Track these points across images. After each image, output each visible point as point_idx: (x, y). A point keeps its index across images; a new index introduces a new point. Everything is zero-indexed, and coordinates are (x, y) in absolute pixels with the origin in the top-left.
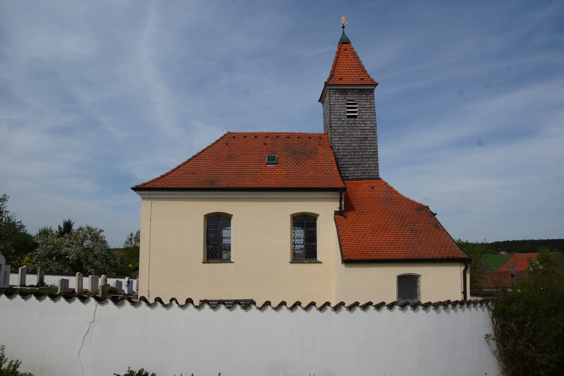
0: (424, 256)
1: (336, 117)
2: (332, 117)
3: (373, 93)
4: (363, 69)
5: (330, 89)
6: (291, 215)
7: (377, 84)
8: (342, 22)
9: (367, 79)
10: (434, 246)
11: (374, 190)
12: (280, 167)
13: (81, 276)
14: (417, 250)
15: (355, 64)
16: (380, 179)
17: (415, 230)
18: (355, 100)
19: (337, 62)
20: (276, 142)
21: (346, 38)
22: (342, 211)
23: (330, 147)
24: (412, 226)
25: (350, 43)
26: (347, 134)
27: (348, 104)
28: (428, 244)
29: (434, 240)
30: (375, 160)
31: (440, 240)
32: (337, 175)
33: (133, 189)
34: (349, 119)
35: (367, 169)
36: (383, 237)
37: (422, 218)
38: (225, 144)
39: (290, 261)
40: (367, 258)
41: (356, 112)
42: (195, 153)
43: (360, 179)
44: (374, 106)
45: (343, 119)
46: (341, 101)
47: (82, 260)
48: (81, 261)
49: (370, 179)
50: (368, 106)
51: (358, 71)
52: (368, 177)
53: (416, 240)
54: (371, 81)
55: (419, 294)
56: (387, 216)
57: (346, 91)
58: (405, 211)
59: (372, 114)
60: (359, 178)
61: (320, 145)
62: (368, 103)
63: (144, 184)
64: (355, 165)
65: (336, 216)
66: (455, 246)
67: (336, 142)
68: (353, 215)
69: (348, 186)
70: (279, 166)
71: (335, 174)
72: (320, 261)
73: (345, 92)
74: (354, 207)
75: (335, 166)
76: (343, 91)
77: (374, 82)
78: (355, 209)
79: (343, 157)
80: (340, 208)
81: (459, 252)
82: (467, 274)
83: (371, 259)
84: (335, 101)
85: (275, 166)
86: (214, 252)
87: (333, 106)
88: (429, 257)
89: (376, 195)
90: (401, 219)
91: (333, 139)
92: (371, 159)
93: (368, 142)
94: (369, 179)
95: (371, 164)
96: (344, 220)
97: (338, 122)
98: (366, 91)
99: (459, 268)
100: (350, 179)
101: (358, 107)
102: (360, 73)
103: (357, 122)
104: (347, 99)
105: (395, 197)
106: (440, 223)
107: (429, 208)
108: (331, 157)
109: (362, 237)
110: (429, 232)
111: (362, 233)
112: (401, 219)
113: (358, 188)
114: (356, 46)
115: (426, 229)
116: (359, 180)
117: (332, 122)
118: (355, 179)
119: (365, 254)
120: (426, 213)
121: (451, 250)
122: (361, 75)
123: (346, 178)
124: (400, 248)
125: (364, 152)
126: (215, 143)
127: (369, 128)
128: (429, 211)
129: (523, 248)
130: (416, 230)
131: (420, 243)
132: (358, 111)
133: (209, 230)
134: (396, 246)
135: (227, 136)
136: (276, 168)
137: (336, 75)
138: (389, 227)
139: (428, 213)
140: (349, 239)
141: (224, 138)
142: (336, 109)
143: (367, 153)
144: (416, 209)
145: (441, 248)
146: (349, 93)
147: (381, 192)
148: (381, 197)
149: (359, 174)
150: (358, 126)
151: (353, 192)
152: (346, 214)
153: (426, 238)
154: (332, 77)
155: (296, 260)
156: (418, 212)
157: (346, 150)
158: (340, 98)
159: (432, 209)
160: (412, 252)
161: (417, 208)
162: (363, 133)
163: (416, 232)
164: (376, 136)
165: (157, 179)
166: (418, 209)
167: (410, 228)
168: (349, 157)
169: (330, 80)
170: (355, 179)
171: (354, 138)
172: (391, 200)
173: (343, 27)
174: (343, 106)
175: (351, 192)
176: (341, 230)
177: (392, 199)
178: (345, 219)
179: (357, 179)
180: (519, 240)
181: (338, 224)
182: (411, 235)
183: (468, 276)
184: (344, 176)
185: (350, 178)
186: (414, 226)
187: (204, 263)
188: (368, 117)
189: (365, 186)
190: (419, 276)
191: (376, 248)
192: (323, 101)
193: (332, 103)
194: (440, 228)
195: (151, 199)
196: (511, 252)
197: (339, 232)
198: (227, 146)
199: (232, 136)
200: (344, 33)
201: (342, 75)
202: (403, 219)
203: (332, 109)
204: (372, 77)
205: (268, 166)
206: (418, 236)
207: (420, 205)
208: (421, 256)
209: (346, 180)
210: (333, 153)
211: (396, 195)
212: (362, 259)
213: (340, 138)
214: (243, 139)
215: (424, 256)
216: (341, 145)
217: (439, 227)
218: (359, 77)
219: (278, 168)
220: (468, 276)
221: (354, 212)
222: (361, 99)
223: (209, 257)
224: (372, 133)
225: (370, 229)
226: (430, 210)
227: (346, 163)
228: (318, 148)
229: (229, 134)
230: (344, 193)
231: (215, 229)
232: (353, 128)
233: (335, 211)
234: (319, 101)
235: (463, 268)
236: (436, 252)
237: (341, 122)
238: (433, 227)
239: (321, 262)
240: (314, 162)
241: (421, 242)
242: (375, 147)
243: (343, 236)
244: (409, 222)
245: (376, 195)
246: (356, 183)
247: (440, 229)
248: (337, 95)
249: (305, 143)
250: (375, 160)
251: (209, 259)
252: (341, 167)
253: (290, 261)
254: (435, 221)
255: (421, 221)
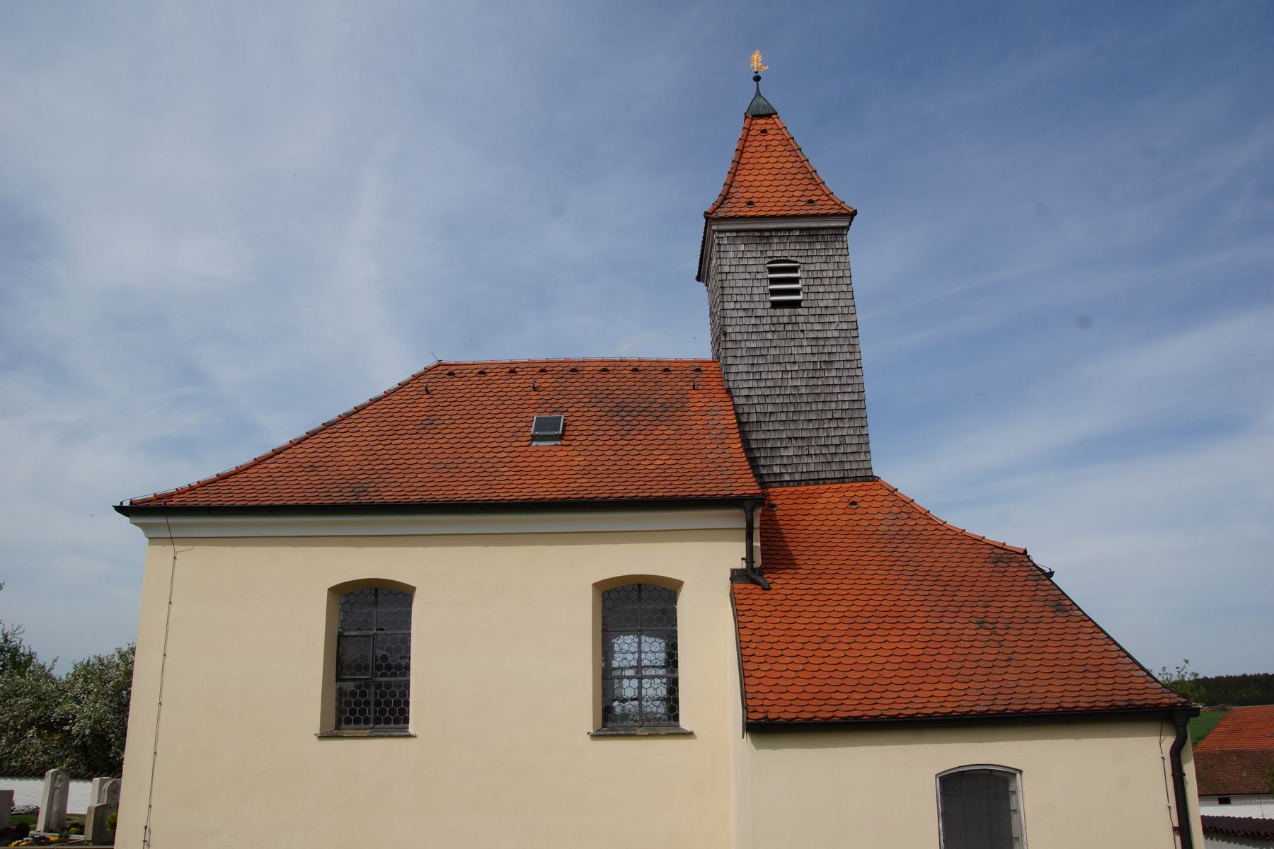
0: (1029, 701)
1: (738, 306)
2: (727, 306)
3: (843, 238)
4: (813, 178)
5: (720, 231)
6: (597, 586)
7: (855, 213)
8: (753, 68)
9: (826, 203)
10: (1057, 669)
11: (857, 511)
12: (570, 445)
13: (60, 780)
14: (1003, 684)
15: (790, 165)
16: (874, 479)
17: (991, 620)
18: (793, 259)
19: (739, 163)
20: (570, 384)
21: (765, 103)
22: (754, 570)
23: (725, 391)
24: (978, 609)
25: (776, 114)
26: (773, 352)
27: (772, 270)
28: (1037, 663)
29: (1057, 650)
30: (858, 423)
31: (1076, 648)
32: (742, 464)
33: (120, 509)
34: (779, 312)
35: (834, 451)
36: (885, 646)
37: (1009, 584)
38: (421, 393)
39: (592, 731)
40: (831, 715)
41: (796, 292)
42: (333, 416)
43: (816, 481)
44: (847, 273)
45: (760, 313)
46: (752, 262)
47: (111, 736)
48: (107, 739)
49: (846, 480)
50: (830, 274)
51: (798, 182)
52: (837, 475)
53: (996, 651)
54: (836, 207)
55: (1017, 839)
56: (898, 582)
57: (767, 234)
58: (955, 565)
59: (843, 295)
60: (812, 478)
61: (694, 389)
62: (831, 266)
63: (158, 498)
64: (799, 440)
65: (737, 586)
66: (1130, 667)
67: (740, 377)
68: (789, 581)
69: (781, 502)
70: (568, 443)
71: (733, 460)
72: (688, 729)
73: (764, 236)
74: (795, 557)
75: (735, 441)
76: (757, 234)
77: (845, 209)
78: (798, 563)
79: (761, 418)
80: (749, 558)
81: (1148, 685)
82: (1187, 763)
83: (842, 718)
84: (735, 262)
85: (556, 445)
86: (358, 703)
87: (730, 277)
88: (1044, 706)
89: (863, 523)
90: (942, 588)
91: (733, 367)
92: (846, 421)
93: (833, 373)
94: (842, 480)
95: (846, 437)
96: (761, 597)
97: (746, 321)
98: (823, 232)
99: (1156, 739)
100: (786, 481)
101: (801, 278)
102: (806, 187)
103: (801, 319)
104: (769, 257)
105: (922, 528)
106: (1068, 598)
107: (1028, 554)
108: (726, 417)
109: (816, 646)
110: (1035, 626)
111: (816, 632)
112: (942, 588)
113: (811, 506)
114: (792, 119)
115: (1026, 615)
116: (812, 482)
117: (728, 321)
118: (799, 482)
119: (823, 702)
120: (1020, 569)
121: (1117, 680)
122: (807, 193)
123: (773, 480)
124: (944, 679)
125: (824, 402)
126: (395, 391)
127: (836, 334)
128: (1030, 564)
129: (1244, 695)
130: (995, 621)
131: (1010, 659)
132: (801, 289)
133: (346, 633)
134: (931, 672)
135: (433, 372)
136: (559, 448)
137: (738, 195)
138: (904, 614)
139: (1028, 569)
140: (772, 652)
141: (423, 377)
142: (740, 283)
143: (833, 406)
144: (988, 560)
145: (1082, 675)
146: (775, 241)
147: (879, 516)
148: (879, 528)
149: (811, 465)
150: (805, 329)
151: (794, 518)
152: (768, 578)
153: (1029, 644)
154: (725, 199)
155: (612, 729)
156: (996, 569)
157: (772, 399)
158: (749, 255)
159: (1041, 559)
160: (984, 691)
161: (992, 556)
162: (820, 348)
163: (995, 628)
164: (857, 356)
165: (203, 485)
166: (995, 560)
167: (974, 614)
168: (779, 419)
169: (718, 207)
170: (801, 480)
171: (794, 363)
172: (910, 537)
173: (757, 79)
174: (759, 276)
175: (789, 518)
176: (748, 625)
177: (913, 532)
178: (764, 592)
179: (807, 482)
180: (1231, 677)
181: (739, 607)
182: (978, 637)
183: (1190, 769)
184: (768, 475)
185: (787, 478)
186: (987, 609)
187: (323, 736)
188: (831, 303)
189: (832, 500)
190: (1015, 774)
191: (862, 681)
192: (707, 278)
193: (726, 269)
194: (1071, 612)
195: (172, 540)
196: (1217, 705)
197: (742, 632)
198: (428, 396)
199: (447, 372)
200: (758, 93)
201: (755, 195)
202: (948, 588)
203: (726, 284)
204: (840, 195)
205: (534, 444)
206: (1000, 638)
207: (1001, 548)
208: (1019, 702)
209: (773, 485)
210: (732, 408)
211: (925, 522)
212: (811, 719)
213: (753, 364)
214: (477, 378)
215: (1029, 701)
216: (755, 384)
217: (1067, 608)
218: (803, 199)
219: (564, 448)
220: (1190, 769)
221: (795, 571)
222: (810, 254)
223: (343, 718)
224: (845, 349)
225: (842, 620)
226: (1032, 562)
227: (772, 435)
228: (688, 396)
229: (440, 368)
230: (758, 512)
231: (364, 633)
232: (790, 335)
233: (733, 571)
234: (698, 279)
235: (1169, 741)
236: (1066, 687)
237: (753, 321)
238: (1047, 609)
239: (689, 734)
240: (673, 432)
241: (1012, 656)
242: (856, 388)
243: (753, 645)
244: (971, 598)
245: (863, 523)
246: (803, 492)
247: (1070, 615)
248: (742, 248)
249: (653, 384)
250: (858, 423)
251: (343, 726)
252: (758, 449)
253: (592, 731)
254: (1050, 592)
255: (1007, 594)
